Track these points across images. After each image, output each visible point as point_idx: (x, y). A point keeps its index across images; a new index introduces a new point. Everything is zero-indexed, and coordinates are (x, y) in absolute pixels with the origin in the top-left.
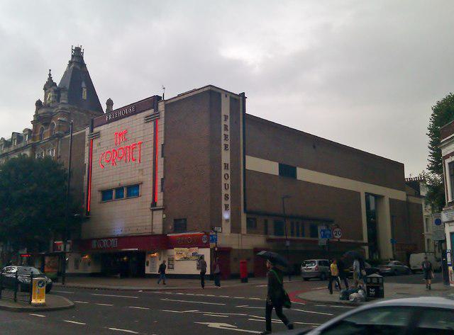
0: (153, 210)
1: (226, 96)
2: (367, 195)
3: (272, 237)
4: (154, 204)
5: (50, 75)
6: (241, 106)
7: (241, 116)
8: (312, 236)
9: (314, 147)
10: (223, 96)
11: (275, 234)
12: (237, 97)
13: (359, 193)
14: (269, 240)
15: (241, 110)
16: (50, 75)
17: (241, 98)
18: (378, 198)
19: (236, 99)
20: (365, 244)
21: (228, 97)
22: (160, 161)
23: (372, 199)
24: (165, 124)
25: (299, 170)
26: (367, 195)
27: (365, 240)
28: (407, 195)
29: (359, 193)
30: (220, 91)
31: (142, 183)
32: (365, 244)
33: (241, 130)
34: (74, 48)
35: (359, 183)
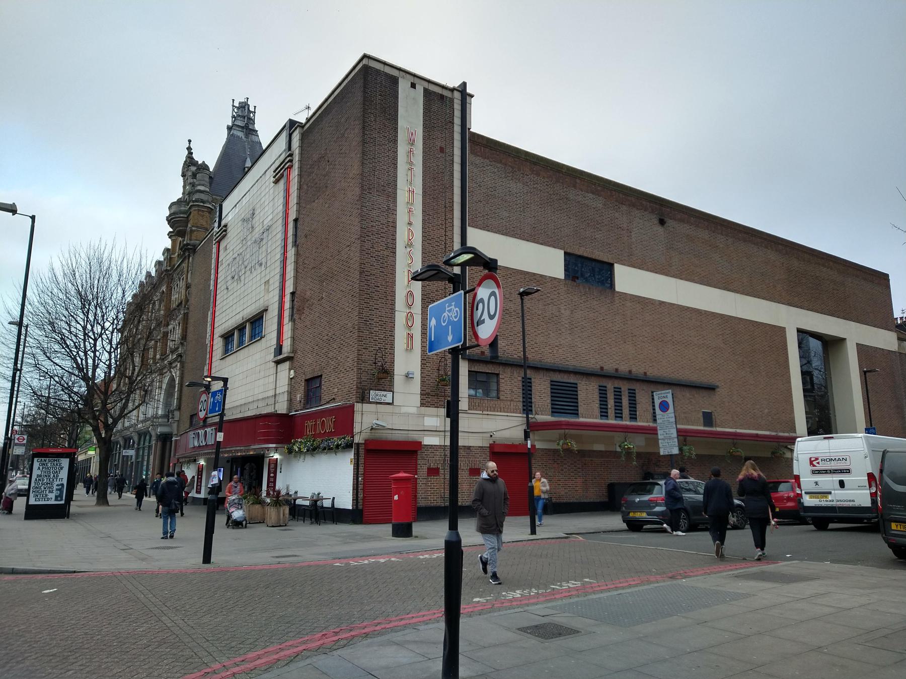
1: (413, 86)
4: (279, 349)
5: (189, 149)
6: (457, 113)
7: (457, 137)
9: (662, 222)
10: (403, 86)
12: (446, 93)
13: (782, 330)
15: (457, 121)
16: (189, 149)
17: (457, 95)
18: (831, 344)
19: (442, 97)
21: (420, 89)
22: (291, 252)
23: (815, 345)
24: (300, 175)
25: (619, 269)
28: (899, 339)
29: (782, 330)
30: (395, 73)
31: (266, 310)
33: (457, 168)
34: (236, 104)
35: (783, 308)
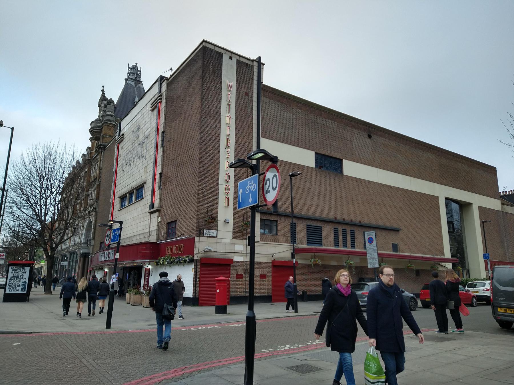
0: (151, 213)
1: (231, 58)
2: (448, 200)
3: (303, 246)
4: (152, 205)
5: (103, 91)
6: (255, 74)
7: (255, 87)
8: (394, 251)
10: (225, 58)
11: (309, 243)
13: (437, 198)
14: (295, 252)
15: (255, 78)
16: (103, 91)
18: (464, 206)
19: (247, 65)
20: (447, 261)
21: (235, 60)
22: (160, 150)
23: (455, 207)
24: (166, 107)
25: (345, 162)
26: (448, 200)
27: (448, 254)
29: (437, 198)
30: (221, 51)
31: (145, 183)
32: (447, 261)
33: (255, 104)
35: (437, 186)
